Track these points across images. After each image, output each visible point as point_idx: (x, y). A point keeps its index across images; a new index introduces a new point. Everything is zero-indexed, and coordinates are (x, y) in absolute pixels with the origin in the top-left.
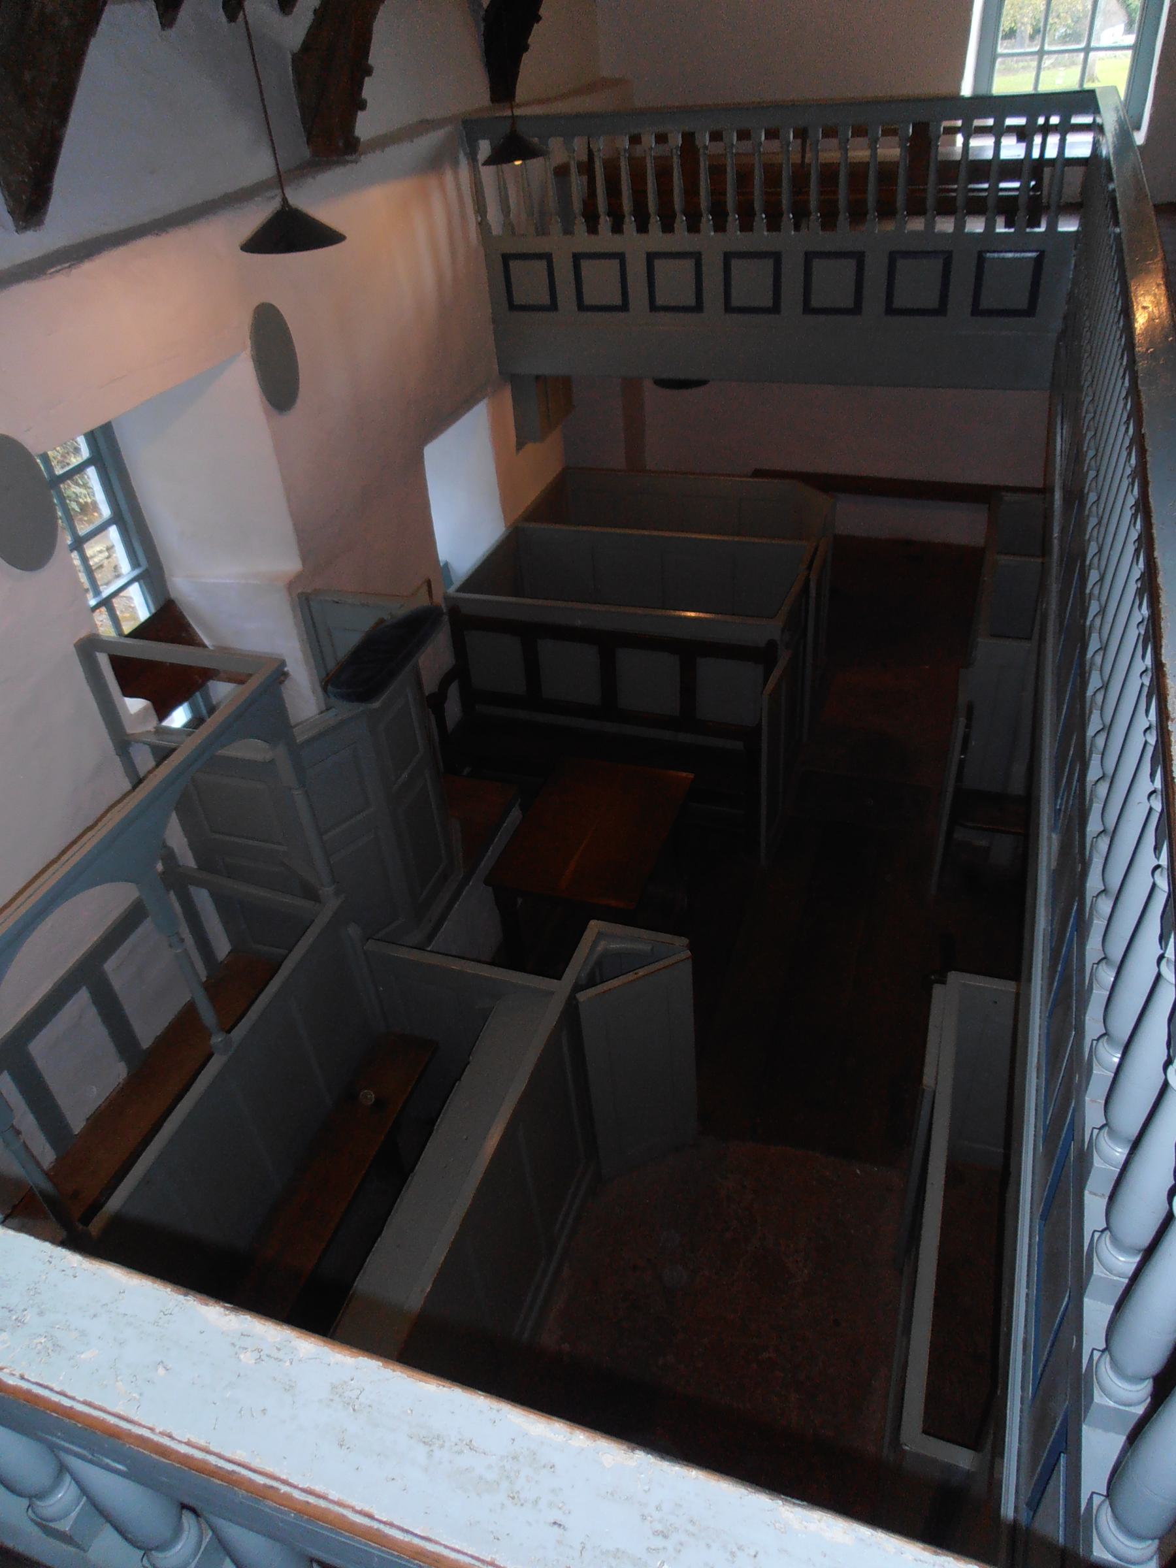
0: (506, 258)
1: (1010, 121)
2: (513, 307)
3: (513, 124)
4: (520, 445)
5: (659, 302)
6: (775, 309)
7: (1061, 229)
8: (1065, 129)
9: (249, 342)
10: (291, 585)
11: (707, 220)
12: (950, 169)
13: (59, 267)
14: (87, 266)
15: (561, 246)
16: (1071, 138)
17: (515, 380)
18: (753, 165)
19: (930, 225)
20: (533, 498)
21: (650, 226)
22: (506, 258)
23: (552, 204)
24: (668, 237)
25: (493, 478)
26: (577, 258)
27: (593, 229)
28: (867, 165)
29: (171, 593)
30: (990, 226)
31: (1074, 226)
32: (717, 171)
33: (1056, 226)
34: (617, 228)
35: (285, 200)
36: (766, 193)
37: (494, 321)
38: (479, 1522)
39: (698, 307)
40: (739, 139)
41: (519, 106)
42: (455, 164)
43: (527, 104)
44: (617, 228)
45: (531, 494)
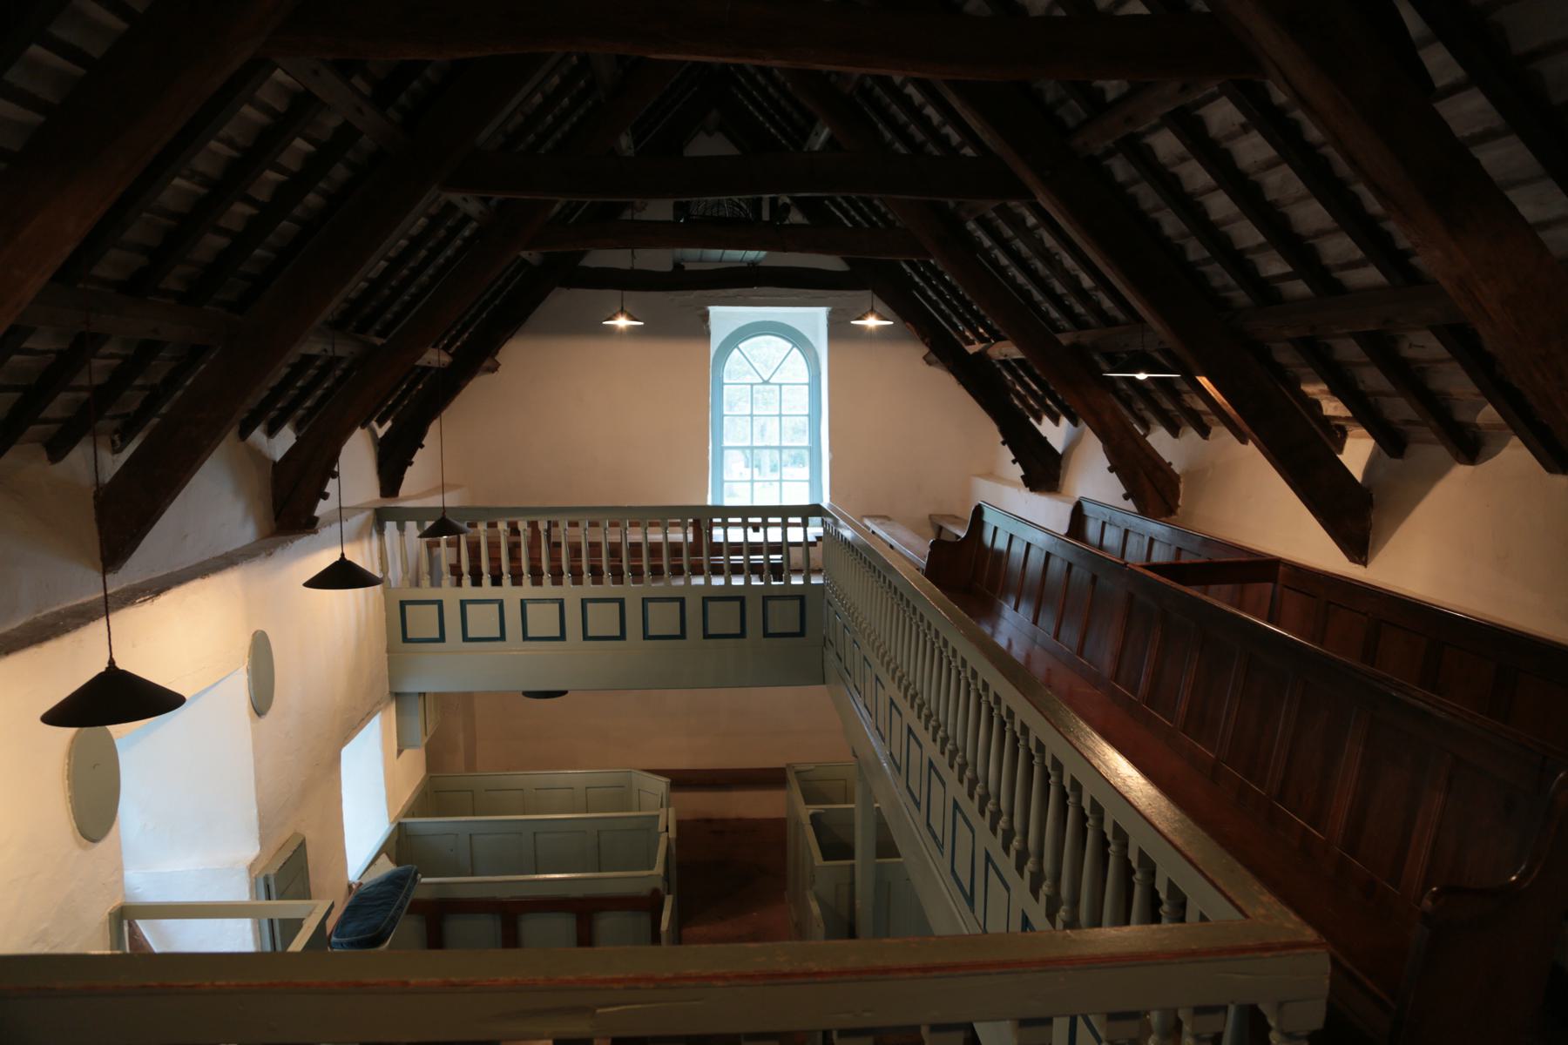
0: (403, 604)
1: (751, 520)
2: (406, 639)
3: (444, 513)
4: (400, 752)
5: (530, 634)
6: (622, 637)
7: (793, 582)
8: (766, 525)
9: (247, 659)
10: (251, 868)
11: (567, 577)
12: (717, 548)
13: (142, 599)
14: (164, 599)
15: (450, 594)
16: (770, 530)
17: (397, 696)
18: (580, 543)
19: (688, 581)
20: (407, 798)
21: (503, 581)
22: (403, 604)
23: (425, 567)
24: (537, 588)
25: (381, 779)
26: (463, 604)
27: (477, 581)
28: (681, 544)
29: (422, 776)
30: (748, 581)
31: (799, 580)
32: (555, 546)
33: (810, 580)
34: (496, 581)
35: (343, 555)
36: (571, 561)
37: (388, 651)
38: (1049, 670)
39: (562, 637)
40: (610, 526)
41: (402, 500)
42: (371, 535)
43: (408, 498)
44: (496, 581)
45: (406, 795)
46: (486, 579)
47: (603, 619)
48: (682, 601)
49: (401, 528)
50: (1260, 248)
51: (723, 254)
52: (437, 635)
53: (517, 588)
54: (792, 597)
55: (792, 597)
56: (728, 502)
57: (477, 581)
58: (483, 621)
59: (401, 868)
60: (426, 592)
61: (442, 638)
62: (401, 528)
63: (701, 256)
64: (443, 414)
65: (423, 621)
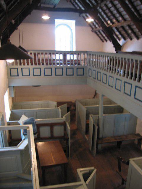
0: (10, 69)
44: (39, 64)
46: (37, 64)
47: (37, 72)
48: (73, 69)
49: (84, 55)
50: (114, 11)
51: (123, 11)
52: (17, 75)
53: (21, 66)
54: (60, 68)
55: (60, 68)
56: (58, 49)
57: (36, 64)
58: (26, 72)
59: (29, 118)
60: (15, 66)
61: (18, 75)
62: (84, 55)
63: (102, 7)
64: (19, 26)
65: (14, 72)
